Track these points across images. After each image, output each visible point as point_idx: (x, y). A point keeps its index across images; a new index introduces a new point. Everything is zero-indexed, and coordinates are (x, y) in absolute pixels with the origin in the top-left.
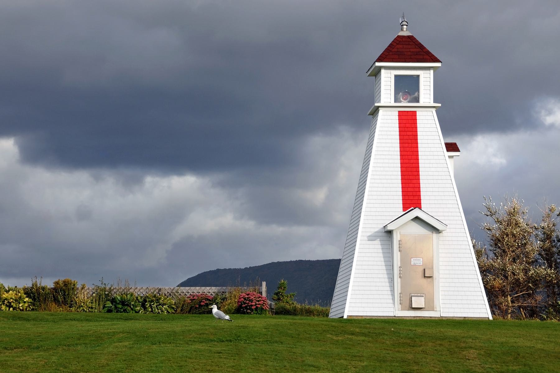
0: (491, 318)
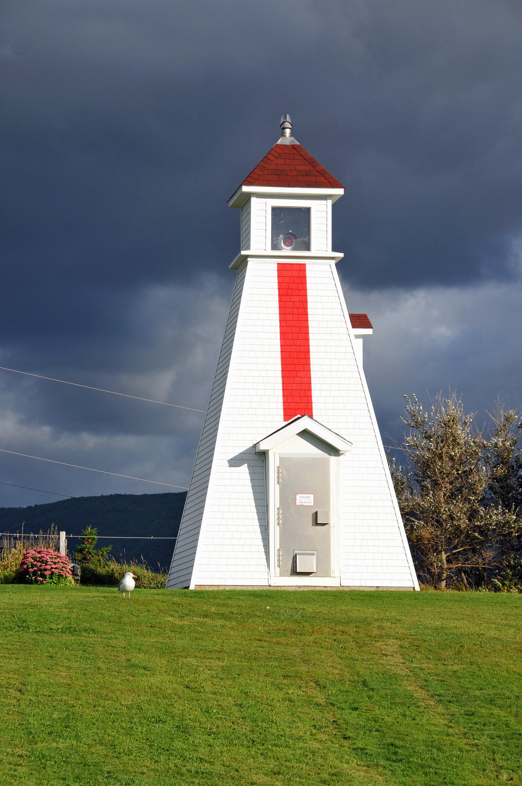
0: (418, 589)
